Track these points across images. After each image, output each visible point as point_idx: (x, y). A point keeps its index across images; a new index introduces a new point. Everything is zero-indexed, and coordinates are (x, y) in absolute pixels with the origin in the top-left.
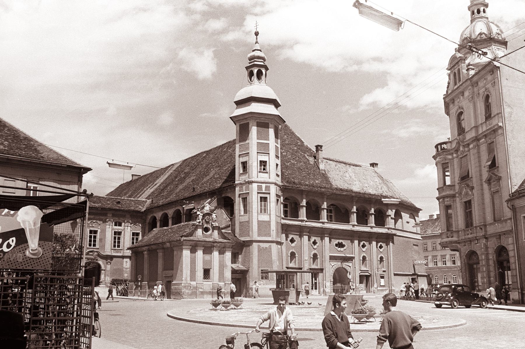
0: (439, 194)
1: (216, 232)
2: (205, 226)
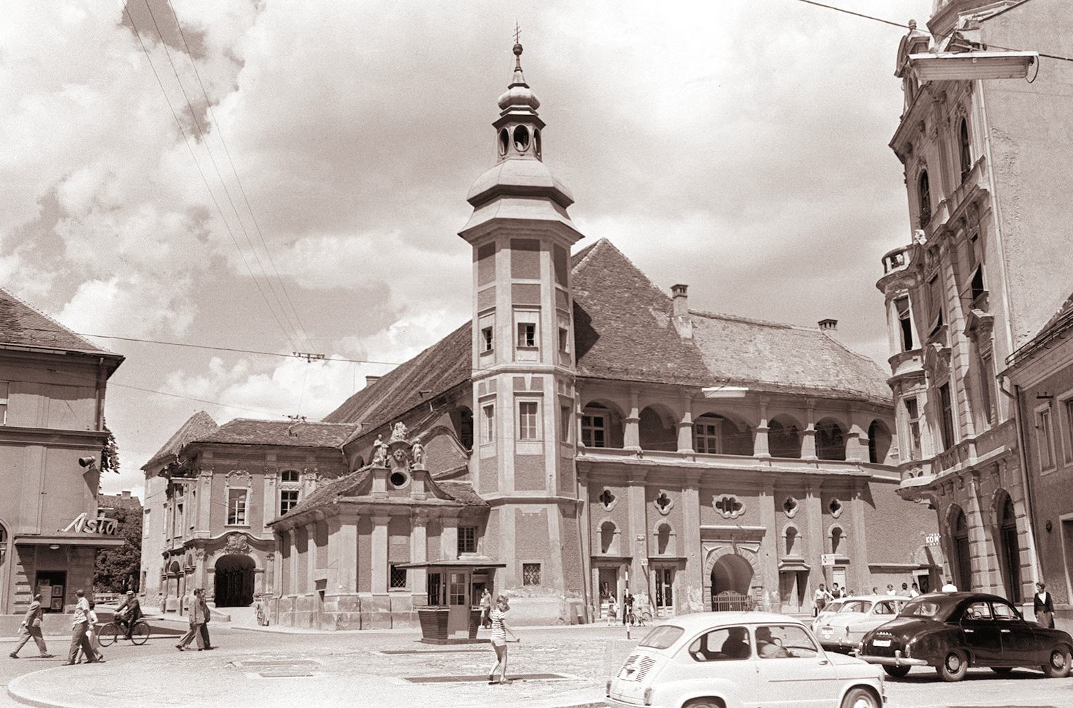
1: (420, 485)
2: (395, 470)
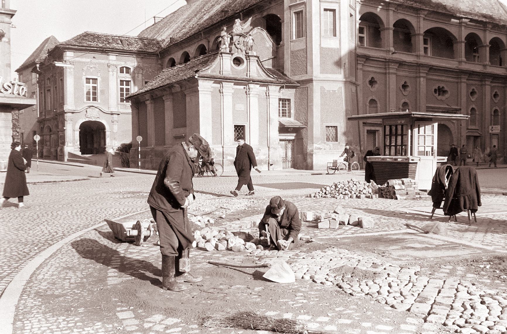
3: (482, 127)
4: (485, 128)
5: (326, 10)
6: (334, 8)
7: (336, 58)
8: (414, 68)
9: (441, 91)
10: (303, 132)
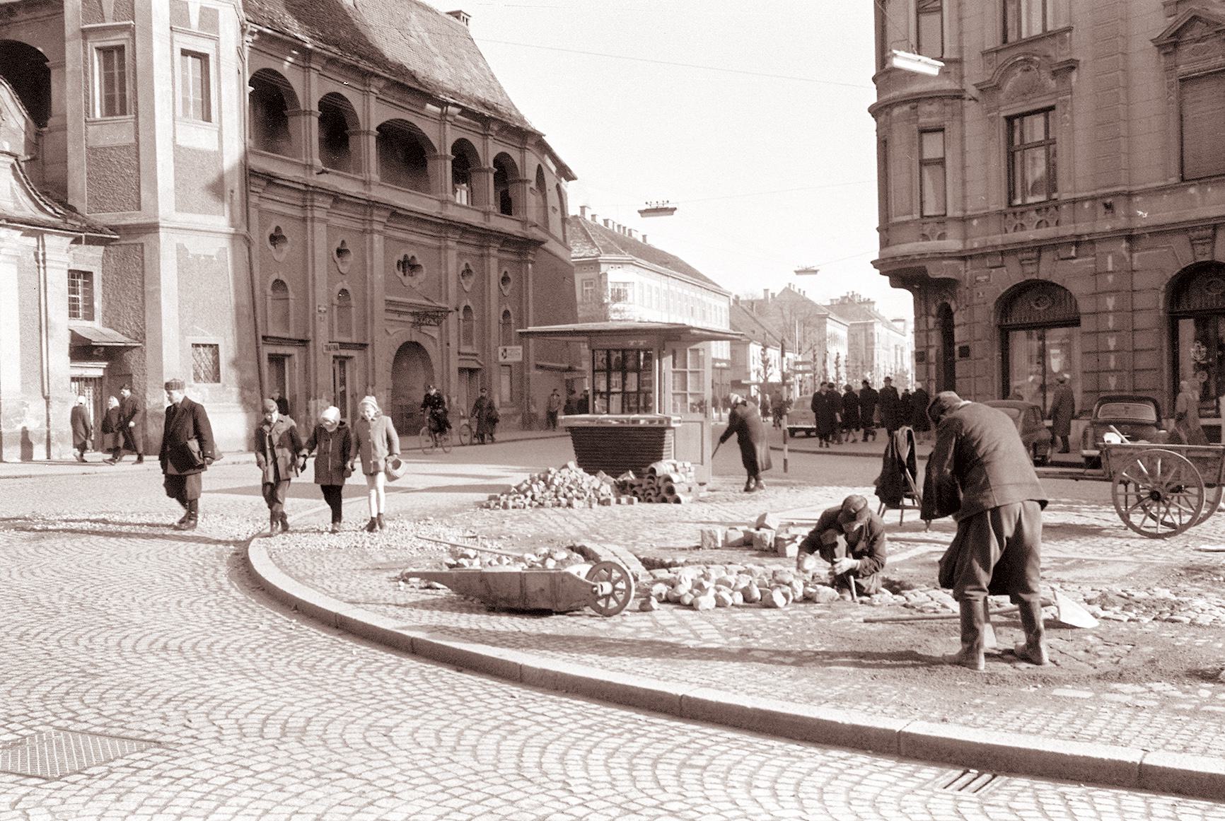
0: (879, 95)
3: (483, 348)
4: (489, 351)
5: (185, 53)
6: (206, 51)
7: (212, 176)
8: (360, 209)
9: (408, 266)
10: (132, 359)
